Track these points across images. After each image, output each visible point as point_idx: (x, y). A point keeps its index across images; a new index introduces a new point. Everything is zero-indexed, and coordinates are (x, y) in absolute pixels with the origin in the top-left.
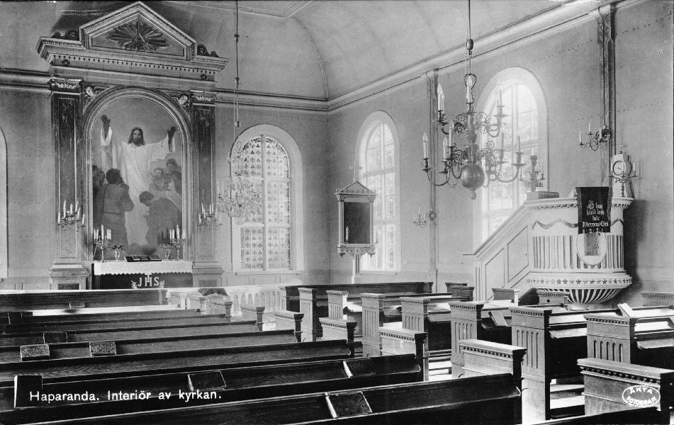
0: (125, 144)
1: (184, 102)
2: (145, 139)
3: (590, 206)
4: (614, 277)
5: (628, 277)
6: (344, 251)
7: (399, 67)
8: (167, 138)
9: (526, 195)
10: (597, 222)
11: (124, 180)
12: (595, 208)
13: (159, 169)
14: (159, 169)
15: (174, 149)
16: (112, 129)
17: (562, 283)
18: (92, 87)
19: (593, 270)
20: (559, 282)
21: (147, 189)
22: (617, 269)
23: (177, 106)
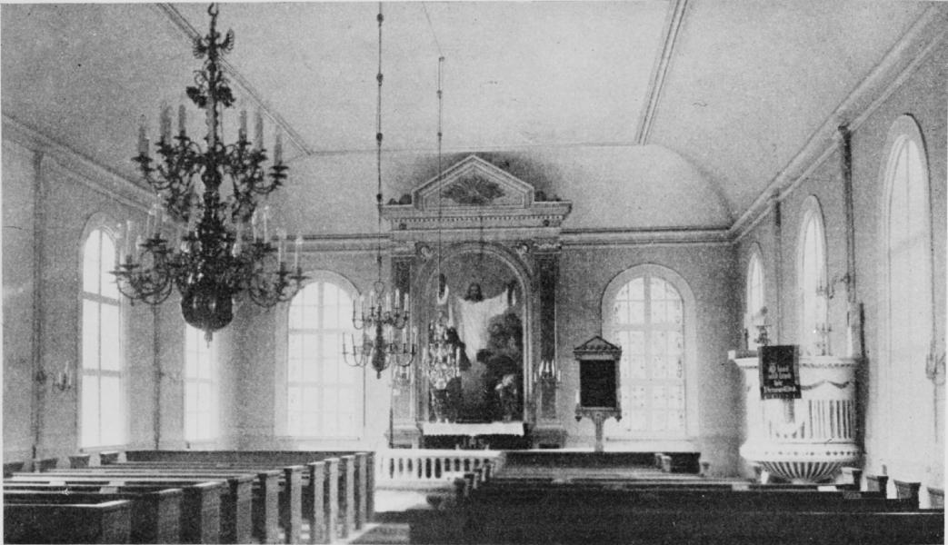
0: (461, 301)
1: (523, 252)
2: (484, 294)
3: (772, 369)
4: (839, 448)
5: (852, 449)
6: (581, 415)
7: (590, 226)
8: (507, 291)
9: (577, 364)
10: (779, 387)
11: (461, 338)
12: (777, 371)
13: (497, 324)
14: (497, 324)
15: (514, 301)
16: (450, 288)
17: (832, 455)
18: (427, 247)
19: (787, 440)
20: (828, 453)
21: (484, 347)
22: (843, 440)
23: (516, 257)
